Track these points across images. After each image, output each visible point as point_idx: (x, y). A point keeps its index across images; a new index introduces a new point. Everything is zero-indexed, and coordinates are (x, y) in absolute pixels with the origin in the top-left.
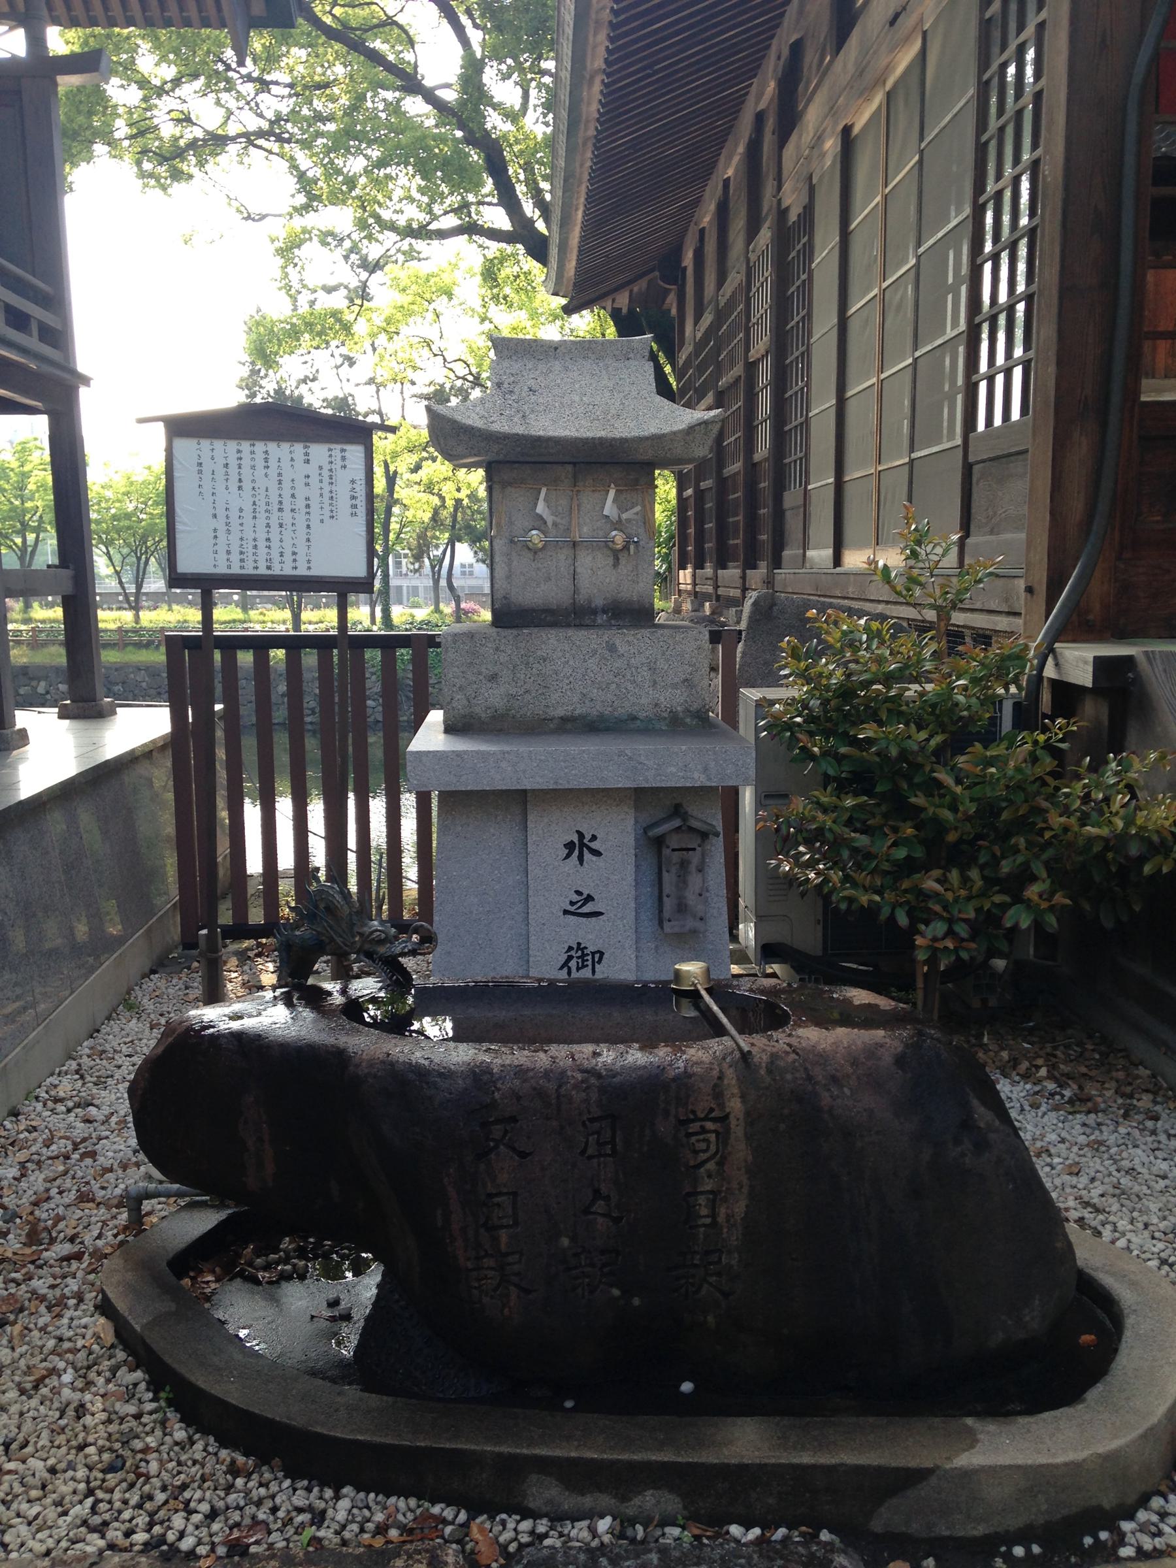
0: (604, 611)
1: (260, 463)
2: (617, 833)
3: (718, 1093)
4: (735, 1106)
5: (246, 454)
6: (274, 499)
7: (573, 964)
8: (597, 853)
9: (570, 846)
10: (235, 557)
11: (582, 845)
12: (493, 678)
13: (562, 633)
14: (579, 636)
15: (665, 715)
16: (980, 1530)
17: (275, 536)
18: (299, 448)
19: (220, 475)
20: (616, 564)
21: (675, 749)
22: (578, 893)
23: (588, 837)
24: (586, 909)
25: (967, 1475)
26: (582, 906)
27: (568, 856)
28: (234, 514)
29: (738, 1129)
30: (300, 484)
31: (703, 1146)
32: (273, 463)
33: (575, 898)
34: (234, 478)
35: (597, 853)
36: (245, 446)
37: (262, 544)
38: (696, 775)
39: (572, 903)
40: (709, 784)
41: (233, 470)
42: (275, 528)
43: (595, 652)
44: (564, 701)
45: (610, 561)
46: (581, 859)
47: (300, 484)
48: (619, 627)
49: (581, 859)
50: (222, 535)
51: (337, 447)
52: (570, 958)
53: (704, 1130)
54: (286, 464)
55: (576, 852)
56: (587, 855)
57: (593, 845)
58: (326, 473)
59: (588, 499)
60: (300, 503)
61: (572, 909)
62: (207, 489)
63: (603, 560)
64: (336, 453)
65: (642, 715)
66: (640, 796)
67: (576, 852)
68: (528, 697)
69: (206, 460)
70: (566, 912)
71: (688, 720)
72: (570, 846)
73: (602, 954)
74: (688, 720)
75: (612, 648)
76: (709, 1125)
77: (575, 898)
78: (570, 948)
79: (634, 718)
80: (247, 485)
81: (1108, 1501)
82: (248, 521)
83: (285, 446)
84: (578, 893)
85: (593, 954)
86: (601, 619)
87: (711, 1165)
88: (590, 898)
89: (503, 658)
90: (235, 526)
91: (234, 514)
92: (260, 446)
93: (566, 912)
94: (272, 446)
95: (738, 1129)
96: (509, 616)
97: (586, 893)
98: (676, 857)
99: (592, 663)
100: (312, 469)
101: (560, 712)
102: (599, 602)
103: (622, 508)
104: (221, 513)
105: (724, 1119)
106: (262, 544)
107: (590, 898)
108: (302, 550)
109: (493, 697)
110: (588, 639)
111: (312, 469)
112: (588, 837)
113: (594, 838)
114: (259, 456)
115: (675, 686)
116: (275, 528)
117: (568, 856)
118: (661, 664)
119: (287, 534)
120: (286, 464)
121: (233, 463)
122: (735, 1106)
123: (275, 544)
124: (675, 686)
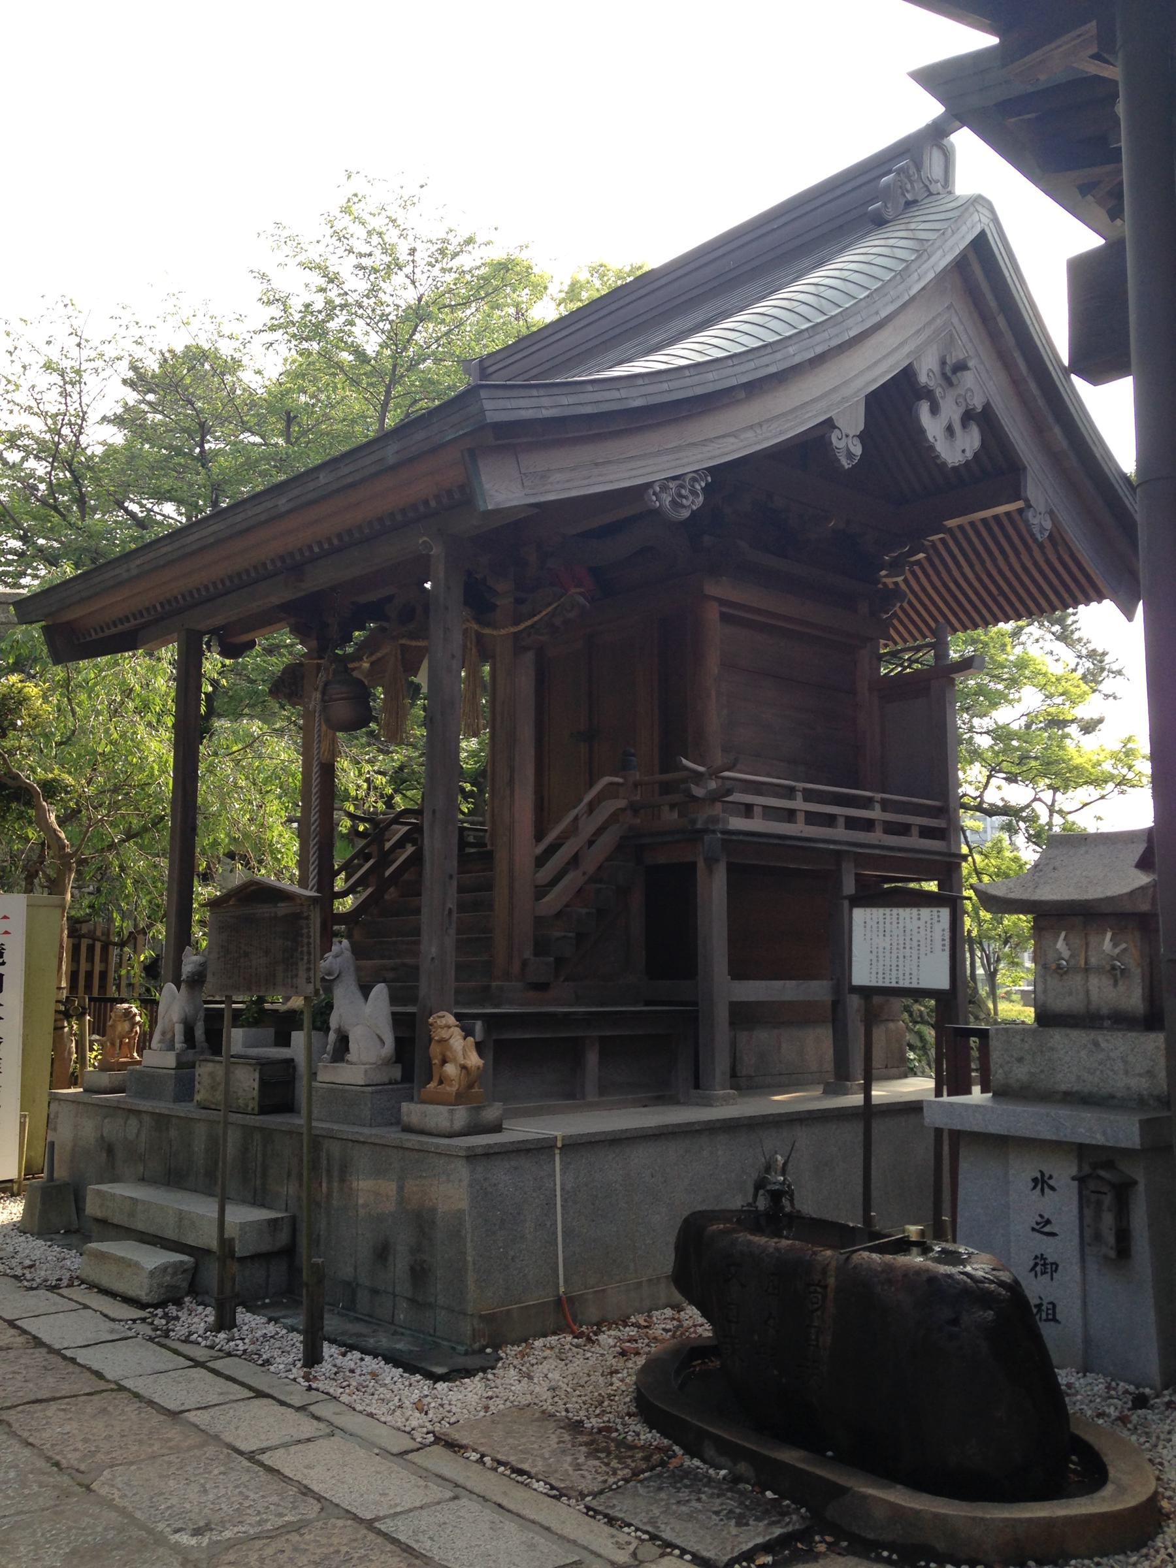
0: (1109, 1018)
1: (895, 921)
2: (1064, 1172)
3: (824, 1271)
4: (831, 1281)
5: (888, 917)
6: (901, 942)
7: (1038, 1269)
8: (1052, 1188)
9: (1035, 1180)
10: (880, 976)
11: (1043, 1182)
12: (1020, 1060)
13: (1064, 1031)
14: (1075, 1034)
15: (1135, 1096)
16: (871, 1536)
17: (901, 964)
18: (915, 911)
19: (875, 929)
20: (1116, 984)
21: (1083, 1115)
22: (1041, 1216)
23: (1047, 1176)
24: (1046, 1229)
25: (865, 1497)
26: (1043, 1227)
27: (1034, 1188)
28: (881, 950)
29: (831, 1295)
30: (915, 932)
31: (814, 1300)
32: (901, 918)
33: (1039, 1220)
34: (881, 929)
35: (1052, 1188)
36: (887, 911)
37: (894, 968)
38: (1098, 1136)
39: (1037, 1223)
40: (1108, 1144)
41: (881, 925)
42: (901, 959)
43: (1085, 1046)
44: (1065, 1080)
45: (1112, 982)
46: (1042, 1190)
47: (915, 932)
48: (1119, 1030)
49: (1042, 1190)
50: (874, 962)
51: (935, 910)
52: (1036, 1265)
53: (816, 1292)
54: (908, 920)
55: (1039, 1186)
56: (1046, 1190)
57: (1051, 1182)
58: (929, 925)
59: (1093, 940)
60: (915, 944)
61: (1037, 1227)
62: (868, 937)
63: (1106, 982)
64: (935, 913)
65: (1119, 1095)
66: (1082, 1151)
67: (1039, 1186)
68: (1043, 1076)
69: (868, 921)
70: (1033, 1229)
71: (1151, 1102)
72: (1035, 1180)
73: (1057, 1266)
74: (1151, 1102)
75: (1096, 1044)
76: (819, 1289)
77: (1039, 1220)
78: (1036, 1257)
79: (1112, 1097)
80: (887, 934)
81: (941, 1546)
82: (888, 954)
83: (908, 910)
84: (1041, 1216)
85: (1052, 1264)
86: (1107, 1023)
87: (819, 1313)
88: (1048, 1222)
89: (1027, 1046)
90: (881, 959)
91: (881, 950)
92: (895, 911)
93: (1033, 1229)
94: (901, 910)
95: (831, 1295)
96: (1044, 1018)
97: (1046, 1216)
98: (1094, 1197)
99: (1083, 1054)
100: (921, 923)
101: (1063, 1087)
102: (1105, 1011)
103: (1115, 945)
104: (875, 951)
105: (825, 1287)
106: (894, 968)
107: (1048, 1222)
108: (915, 972)
109: (1021, 1073)
110: (1079, 1036)
111: (921, 923)
112: (1047, 1176)
113: (1051, 1177)
114: (895, 916)
115: (1140, 1075)
116: (901, 959)
117: (1034, 1188)
118: (1131, 1058)
119: (888, 963)
120: (908, 920)
121: (881, 921)
122: (831, 1281)
123: (901, 968)
124: (1140, 1075)
